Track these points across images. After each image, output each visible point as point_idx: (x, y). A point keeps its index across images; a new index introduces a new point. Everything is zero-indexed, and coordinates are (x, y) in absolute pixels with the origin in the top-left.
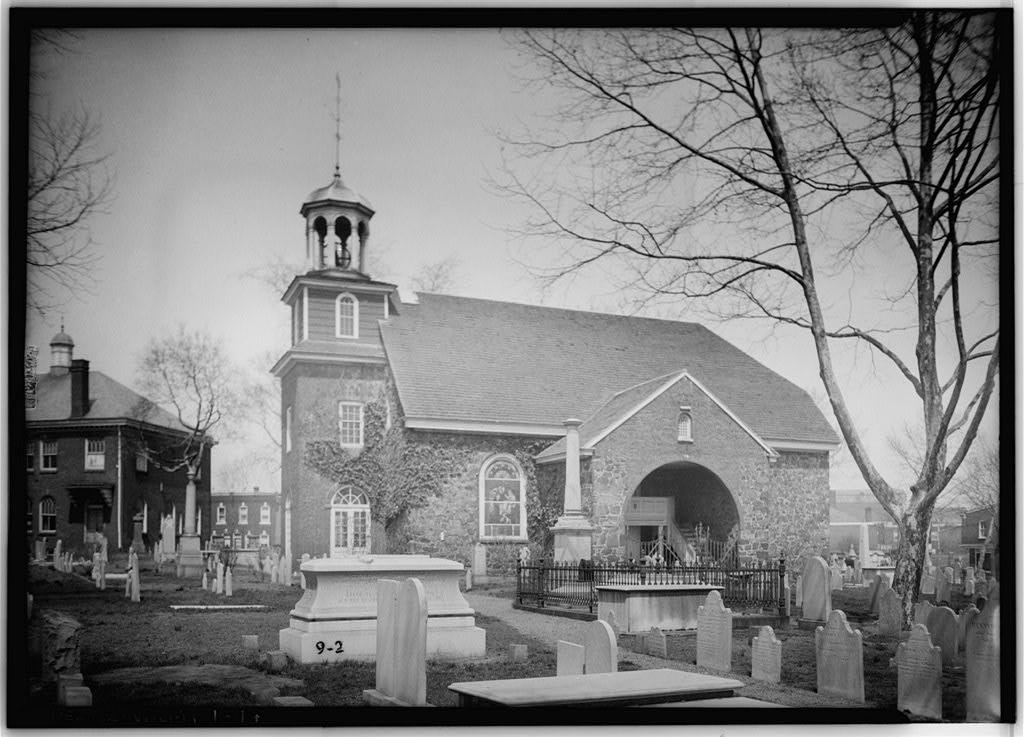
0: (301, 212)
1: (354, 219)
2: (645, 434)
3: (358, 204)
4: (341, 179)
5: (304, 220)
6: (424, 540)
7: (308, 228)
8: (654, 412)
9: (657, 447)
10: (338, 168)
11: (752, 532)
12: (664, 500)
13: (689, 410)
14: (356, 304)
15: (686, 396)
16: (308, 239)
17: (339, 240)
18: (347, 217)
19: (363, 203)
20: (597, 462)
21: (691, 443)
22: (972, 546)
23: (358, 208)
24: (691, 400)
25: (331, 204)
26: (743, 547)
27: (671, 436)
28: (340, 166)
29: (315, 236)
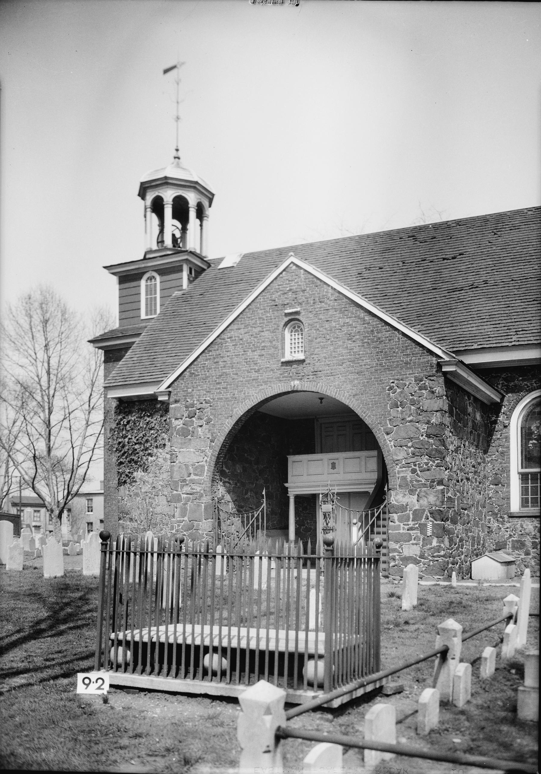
0: (139, 195)
1: (192, 198)
2: (235, 360)
3: (197, 183)
4: (181, 160)
5: (143, 202)
6: (131, 520)
7: (146, 209)
8: (246, 326)
9: (254, 375)
10: (177, 150)
11: (412, 492)
12: (291, 459)
13: (297, 313)
14: (158, 278)
15: (295, 292)
16: (146, 224)
17: (179, 225)
18: (183, 195)
19: (200, 182)
20: (175, 409)
21: (303, 361)
22: (514, 618)
23: (194, 186)
24: (301, 297)
25: (165, 182)
26: (395, 516)
27: (272, 356)
28: (179, 148)
29: (154, 219)
